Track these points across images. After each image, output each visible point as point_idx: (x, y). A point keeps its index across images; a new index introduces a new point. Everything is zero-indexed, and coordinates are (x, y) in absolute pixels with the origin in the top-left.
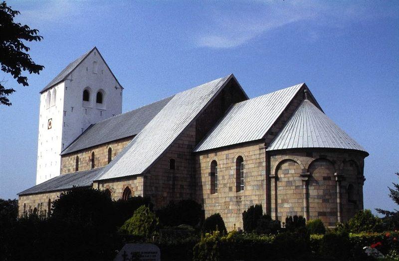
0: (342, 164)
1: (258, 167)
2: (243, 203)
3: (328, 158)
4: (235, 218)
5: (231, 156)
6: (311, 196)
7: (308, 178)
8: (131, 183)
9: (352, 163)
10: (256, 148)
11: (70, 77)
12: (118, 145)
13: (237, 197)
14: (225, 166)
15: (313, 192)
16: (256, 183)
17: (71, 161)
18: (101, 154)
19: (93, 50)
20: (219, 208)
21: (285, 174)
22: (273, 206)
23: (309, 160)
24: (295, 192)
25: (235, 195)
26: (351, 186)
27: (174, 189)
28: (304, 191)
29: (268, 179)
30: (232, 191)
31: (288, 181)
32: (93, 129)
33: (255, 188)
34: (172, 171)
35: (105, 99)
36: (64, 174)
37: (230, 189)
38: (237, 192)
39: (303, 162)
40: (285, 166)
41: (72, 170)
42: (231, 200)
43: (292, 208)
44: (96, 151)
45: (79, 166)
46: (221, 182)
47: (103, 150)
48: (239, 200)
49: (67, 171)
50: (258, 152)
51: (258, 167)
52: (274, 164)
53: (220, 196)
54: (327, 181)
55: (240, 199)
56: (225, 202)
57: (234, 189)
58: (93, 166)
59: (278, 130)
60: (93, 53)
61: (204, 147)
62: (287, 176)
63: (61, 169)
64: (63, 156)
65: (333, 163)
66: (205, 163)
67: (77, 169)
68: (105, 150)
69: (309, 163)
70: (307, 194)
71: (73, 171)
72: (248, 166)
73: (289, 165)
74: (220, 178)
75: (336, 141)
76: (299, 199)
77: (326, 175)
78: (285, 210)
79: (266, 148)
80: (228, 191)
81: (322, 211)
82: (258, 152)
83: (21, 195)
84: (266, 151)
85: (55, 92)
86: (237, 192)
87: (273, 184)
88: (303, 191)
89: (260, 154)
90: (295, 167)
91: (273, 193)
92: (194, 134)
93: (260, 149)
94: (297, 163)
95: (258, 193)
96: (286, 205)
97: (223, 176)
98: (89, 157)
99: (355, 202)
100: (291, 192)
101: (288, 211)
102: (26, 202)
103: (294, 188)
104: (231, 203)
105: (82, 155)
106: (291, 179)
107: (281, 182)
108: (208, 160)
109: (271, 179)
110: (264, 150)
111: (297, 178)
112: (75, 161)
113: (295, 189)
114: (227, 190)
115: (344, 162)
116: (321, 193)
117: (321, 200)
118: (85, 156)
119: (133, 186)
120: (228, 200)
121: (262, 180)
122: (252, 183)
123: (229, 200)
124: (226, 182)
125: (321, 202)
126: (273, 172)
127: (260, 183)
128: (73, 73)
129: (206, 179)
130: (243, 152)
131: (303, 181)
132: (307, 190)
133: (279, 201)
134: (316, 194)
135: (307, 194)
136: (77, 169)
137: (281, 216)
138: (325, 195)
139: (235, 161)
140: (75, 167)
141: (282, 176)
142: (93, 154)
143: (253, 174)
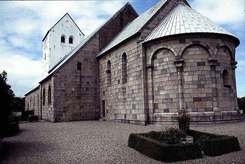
0: (216, 50)
1: (137, 59)
2: (127, 93)
7: (180, 64)
9: (226, 48)
11: (52, 30)
15: (187, 78)
16: (135, 74)
19: (66, 15)
22: (150, 94)
23: (183, 47)
26: (225, 72)
27: (80, 85)
31: (163, 69)
34: (79, 71)
35: (74, 41)
40: (160, 55)
42: (120, 91)
43: (168, 95)
51: (137, 59)
52: (150, 54)
55: (125, 89)
56: (116, 93)
57: (121, 81)
59: (154, 26)
60: (66, 15)
62: (161, 64)
65: (206, 49)
69: (183, 49)
70: (182, 80)
72: (131, 59)
75: (174, 122)
78: (161, 97)
82: (136, 46)
83: (26, 95)
84: (142, 43)
87: (150, 73)
89: (138, 47)
93: (138, 43)
95: (137, 83)
96: (162, 93)
99: (229, 87)
100: (167, 79)
103: (169, 75)
104: (120, 94)
106: (166, 67)
107: (157, 70)
108: (106, 60)
109: (148, 68)
111: (171, 66)
113: (170, 76)
115: (218, 47)
116: (196, 78)
120: (117, 91)
121: (140, 71)
122: (133, 75)
128: (54, 27)
129: (104, 75)
131: (177, 68)
134: (191, 80)
138: (199, 81)
141: (158, 65)
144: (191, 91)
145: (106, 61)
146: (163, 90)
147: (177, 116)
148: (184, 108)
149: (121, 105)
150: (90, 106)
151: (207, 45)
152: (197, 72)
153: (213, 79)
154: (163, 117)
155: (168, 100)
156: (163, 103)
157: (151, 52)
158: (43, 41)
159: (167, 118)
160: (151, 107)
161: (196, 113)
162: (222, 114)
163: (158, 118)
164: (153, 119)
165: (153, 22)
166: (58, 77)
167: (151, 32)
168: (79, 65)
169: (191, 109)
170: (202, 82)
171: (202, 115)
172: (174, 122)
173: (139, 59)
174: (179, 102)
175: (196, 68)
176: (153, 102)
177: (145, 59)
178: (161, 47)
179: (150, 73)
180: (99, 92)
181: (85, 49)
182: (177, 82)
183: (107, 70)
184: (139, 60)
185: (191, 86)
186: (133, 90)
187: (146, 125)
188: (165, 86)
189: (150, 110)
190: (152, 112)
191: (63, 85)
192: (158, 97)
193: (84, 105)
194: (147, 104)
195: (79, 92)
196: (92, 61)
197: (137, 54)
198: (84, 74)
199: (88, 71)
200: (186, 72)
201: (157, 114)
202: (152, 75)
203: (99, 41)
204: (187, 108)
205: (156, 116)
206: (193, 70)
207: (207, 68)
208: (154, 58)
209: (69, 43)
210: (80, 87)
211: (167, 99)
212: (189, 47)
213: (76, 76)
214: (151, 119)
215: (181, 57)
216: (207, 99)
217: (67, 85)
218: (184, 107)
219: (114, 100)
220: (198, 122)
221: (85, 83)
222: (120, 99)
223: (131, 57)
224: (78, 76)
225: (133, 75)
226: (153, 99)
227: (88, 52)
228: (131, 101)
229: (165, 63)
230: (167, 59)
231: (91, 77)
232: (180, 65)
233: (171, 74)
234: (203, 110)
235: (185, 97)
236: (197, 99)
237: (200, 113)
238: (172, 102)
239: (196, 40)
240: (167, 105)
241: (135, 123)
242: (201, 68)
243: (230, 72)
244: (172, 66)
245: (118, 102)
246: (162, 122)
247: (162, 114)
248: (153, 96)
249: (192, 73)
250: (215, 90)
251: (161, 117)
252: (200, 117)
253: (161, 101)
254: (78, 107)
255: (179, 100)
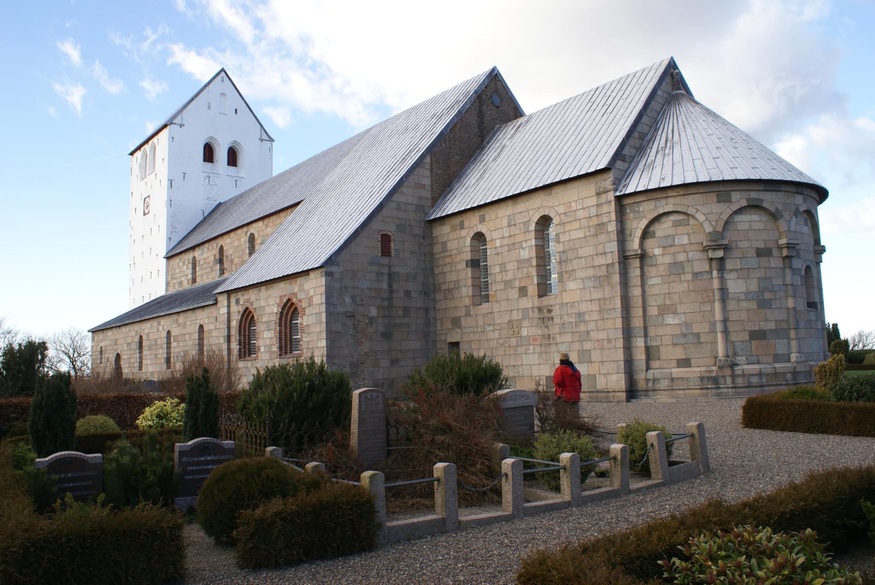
2: (557, 320)
3: (765, 205)
4: (536, 356)
5: (520, 219)
6: (730, 296)
7: (720, 249)
8: (296, 290)
10: (588, 189)
12: (267, 226)
13: (540, 309)
14: (506, 241)
15: (736, 286)
16: (590, 272)
17: (183, 265)
18: (235, 244)
20: (496, 334)
21: (664, 247)
22: (637, 322)
23: (725, 210)
24: (691, 288)
25: (536, 304)
26: (808, 268)
27: (390, 299)
28: (716, 284)
29: (624, 259)
30: (526, 295)
31: (675, 263)
32: (221, 209)
33: (589, 284)
34: (385, 260)
35: (242, 159)
36: (172, 291)
37: (523, 291)
38: (540, 296)
39: (707, 214)
40: (663, 229)
41: (185, 283)
43: (687, 324)
44: (226, 242)
45: (198, 274)
46: (499, 278)
47: (239, 239)
48: (546, 315)
49: (177, 286)
50: (594, 201)
53: (495, 310)
54: (765, 259)
55: (550, 311)
56: (510, 321)
57: (533, 290)
58: (222, 272)
61: (453, 205)
62: (668, 250)
63: (168, 284)
64: (168, 258)
65: (775, 216)
66: (457, 242)
67: (194, 280)
68: (242, 238)
69: (725, 217)
70: (723, 290)
71: (186, 286)
73: (676, 224)
74: (494, 270)
75: (708, 388)
76: (703, 303)
77: (761, 245)
78: (669, 331)
79: (616, 190)
80: (517, 296)
81: (757, 328)
82: (594, 201)
85: (154, 149)
86: (540, 296)
87: (635, 271)
88: (712, 284)
89: (598, 205)
90: (688, 229)
91: (636, 292)
92: (426, 181)
93: (598, 194)
94: (696, 219)
95: (597, 295)
96: (670, 320)
97: (503, 265)
98: (215, 256)
100: (683, 287)
101: (679, 332)
102: (102, 344)
103: (689, 277)
104: (526, 323)
105: (203, 253)
106: (681, 257)
107: (655, 265)
108: (463, 233)
109: (629, 261)
110: (611, 196)
112: (190, 266)
114: (514, 294)
116: (753, 286)
117: (755, 303)
118: (207, 255)
119: (301, 296)
120: (516, 316)
121: (608, 265)
122: (580, 274)
123: (520, 317)
124: (510, 276)
125: (756, 307)
126: (634, 245)
127: (603, 272)
130: (553, 205)
132: (722, 279)
133: (653, 311)
134: (744, 290)
135: (723, 290)
136: (194, 280)
137: (658, 347)
138: (762, 291)
139: (532, 227)
140: (190, 276)
141: (657, 251)
142: (221, 249)
143: (581, 252)
144: (744, 316)
145: (467, 235)
146: (675, 313)
147: (714, 374)
148: (728, 356)
149: (534, 353)
150: (414, 359)
151: (777, 209)
152: (757, 271)
153: (790, 287)
154: (678, 379)
155: (689, 337)
156: (674, 345)
157: (640, 219)
158: (132, 154)
159: (687, 379)
160: (640, 355)
161: (757, 366)
162: (808, 369)
163: (662, 381)
164: (647, 385)
165: (631, 142)
166: (337, 276)
167: (629, 168)
168: (386, 240)
169: (744, 358)
170: (767, 296)
171: (770, 371)
172: (708, 388)
173: (604, 235)
174: (715, 342)
175: (753, 262)
176: (646, 342)
177: (622, 236)
178: (669, 208)
179: (638, 272)
180: (435, 319)
181: (397, 197)
182: (710, 294)
183: (469, 258)
184: (603, 238)
185: (744, 305)
186: (580, 315)
187: (628, 400)
188: (680, 303)
189: (636, 363)
190: (644, 368)
191: (348, 300)
192: (660, 331)
193: (400, 355)
194: (628, 348)
195: (386, 321)
196: (417, 231)
197: (595, 221)
198: (397, 270)
199: (405, 261)
200: (731, 270)
201: (659, 371)
202: (643, 275)
203: (432, 176)
204: (735, 354)
205: (657, 376)
206: (747, 266)
207: (776, 262)
208: (646, 234)
209: (205, 160)
210: (390, 306)
211: (685, 335)
212: (738, 212)
213: (379, 274)
214: (641, 385)
215: (721, 235)
216: (781, 333)
217: (358, 299)
218: (730, 354)
219: (501, 342)
220: (762, 386)
221: (401, 294)
222: (528, 336)
223: (573, 228)
224: (382, 273)
225: (580, 274)
226: (646, 336)
227: (406, 204)
228: (573, 342)
229: (679, 249)
230: (685, 240)
231: (415, 278)
232: (720, 254)
233: (695, 274)
234: (770, 359)
235: (730, 329)
236: (757, 335)
237: (766, 368)
238: (699, 343)
239: (754, 195)
240: (685, 349)
241: (590, 397)
242: (764, 260)
243: (814, 269)
244: (699, 255)
245: (521, 346)
246: (673, 390)
247: (674, 370)
248: (645, 329)
249: (744, 273)
250: (792, 313)
251: (672, 380)
252: (767, 375)
253: (667, 340)
254: (385, 363)
255: (715, 338)
